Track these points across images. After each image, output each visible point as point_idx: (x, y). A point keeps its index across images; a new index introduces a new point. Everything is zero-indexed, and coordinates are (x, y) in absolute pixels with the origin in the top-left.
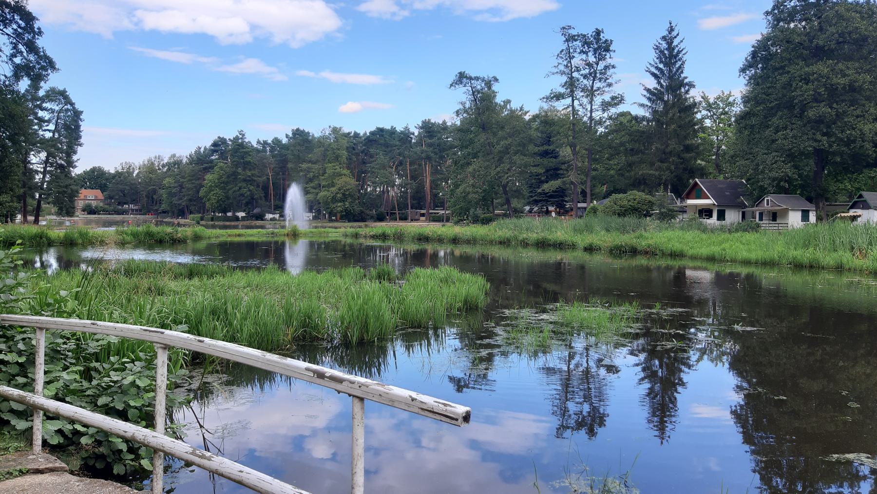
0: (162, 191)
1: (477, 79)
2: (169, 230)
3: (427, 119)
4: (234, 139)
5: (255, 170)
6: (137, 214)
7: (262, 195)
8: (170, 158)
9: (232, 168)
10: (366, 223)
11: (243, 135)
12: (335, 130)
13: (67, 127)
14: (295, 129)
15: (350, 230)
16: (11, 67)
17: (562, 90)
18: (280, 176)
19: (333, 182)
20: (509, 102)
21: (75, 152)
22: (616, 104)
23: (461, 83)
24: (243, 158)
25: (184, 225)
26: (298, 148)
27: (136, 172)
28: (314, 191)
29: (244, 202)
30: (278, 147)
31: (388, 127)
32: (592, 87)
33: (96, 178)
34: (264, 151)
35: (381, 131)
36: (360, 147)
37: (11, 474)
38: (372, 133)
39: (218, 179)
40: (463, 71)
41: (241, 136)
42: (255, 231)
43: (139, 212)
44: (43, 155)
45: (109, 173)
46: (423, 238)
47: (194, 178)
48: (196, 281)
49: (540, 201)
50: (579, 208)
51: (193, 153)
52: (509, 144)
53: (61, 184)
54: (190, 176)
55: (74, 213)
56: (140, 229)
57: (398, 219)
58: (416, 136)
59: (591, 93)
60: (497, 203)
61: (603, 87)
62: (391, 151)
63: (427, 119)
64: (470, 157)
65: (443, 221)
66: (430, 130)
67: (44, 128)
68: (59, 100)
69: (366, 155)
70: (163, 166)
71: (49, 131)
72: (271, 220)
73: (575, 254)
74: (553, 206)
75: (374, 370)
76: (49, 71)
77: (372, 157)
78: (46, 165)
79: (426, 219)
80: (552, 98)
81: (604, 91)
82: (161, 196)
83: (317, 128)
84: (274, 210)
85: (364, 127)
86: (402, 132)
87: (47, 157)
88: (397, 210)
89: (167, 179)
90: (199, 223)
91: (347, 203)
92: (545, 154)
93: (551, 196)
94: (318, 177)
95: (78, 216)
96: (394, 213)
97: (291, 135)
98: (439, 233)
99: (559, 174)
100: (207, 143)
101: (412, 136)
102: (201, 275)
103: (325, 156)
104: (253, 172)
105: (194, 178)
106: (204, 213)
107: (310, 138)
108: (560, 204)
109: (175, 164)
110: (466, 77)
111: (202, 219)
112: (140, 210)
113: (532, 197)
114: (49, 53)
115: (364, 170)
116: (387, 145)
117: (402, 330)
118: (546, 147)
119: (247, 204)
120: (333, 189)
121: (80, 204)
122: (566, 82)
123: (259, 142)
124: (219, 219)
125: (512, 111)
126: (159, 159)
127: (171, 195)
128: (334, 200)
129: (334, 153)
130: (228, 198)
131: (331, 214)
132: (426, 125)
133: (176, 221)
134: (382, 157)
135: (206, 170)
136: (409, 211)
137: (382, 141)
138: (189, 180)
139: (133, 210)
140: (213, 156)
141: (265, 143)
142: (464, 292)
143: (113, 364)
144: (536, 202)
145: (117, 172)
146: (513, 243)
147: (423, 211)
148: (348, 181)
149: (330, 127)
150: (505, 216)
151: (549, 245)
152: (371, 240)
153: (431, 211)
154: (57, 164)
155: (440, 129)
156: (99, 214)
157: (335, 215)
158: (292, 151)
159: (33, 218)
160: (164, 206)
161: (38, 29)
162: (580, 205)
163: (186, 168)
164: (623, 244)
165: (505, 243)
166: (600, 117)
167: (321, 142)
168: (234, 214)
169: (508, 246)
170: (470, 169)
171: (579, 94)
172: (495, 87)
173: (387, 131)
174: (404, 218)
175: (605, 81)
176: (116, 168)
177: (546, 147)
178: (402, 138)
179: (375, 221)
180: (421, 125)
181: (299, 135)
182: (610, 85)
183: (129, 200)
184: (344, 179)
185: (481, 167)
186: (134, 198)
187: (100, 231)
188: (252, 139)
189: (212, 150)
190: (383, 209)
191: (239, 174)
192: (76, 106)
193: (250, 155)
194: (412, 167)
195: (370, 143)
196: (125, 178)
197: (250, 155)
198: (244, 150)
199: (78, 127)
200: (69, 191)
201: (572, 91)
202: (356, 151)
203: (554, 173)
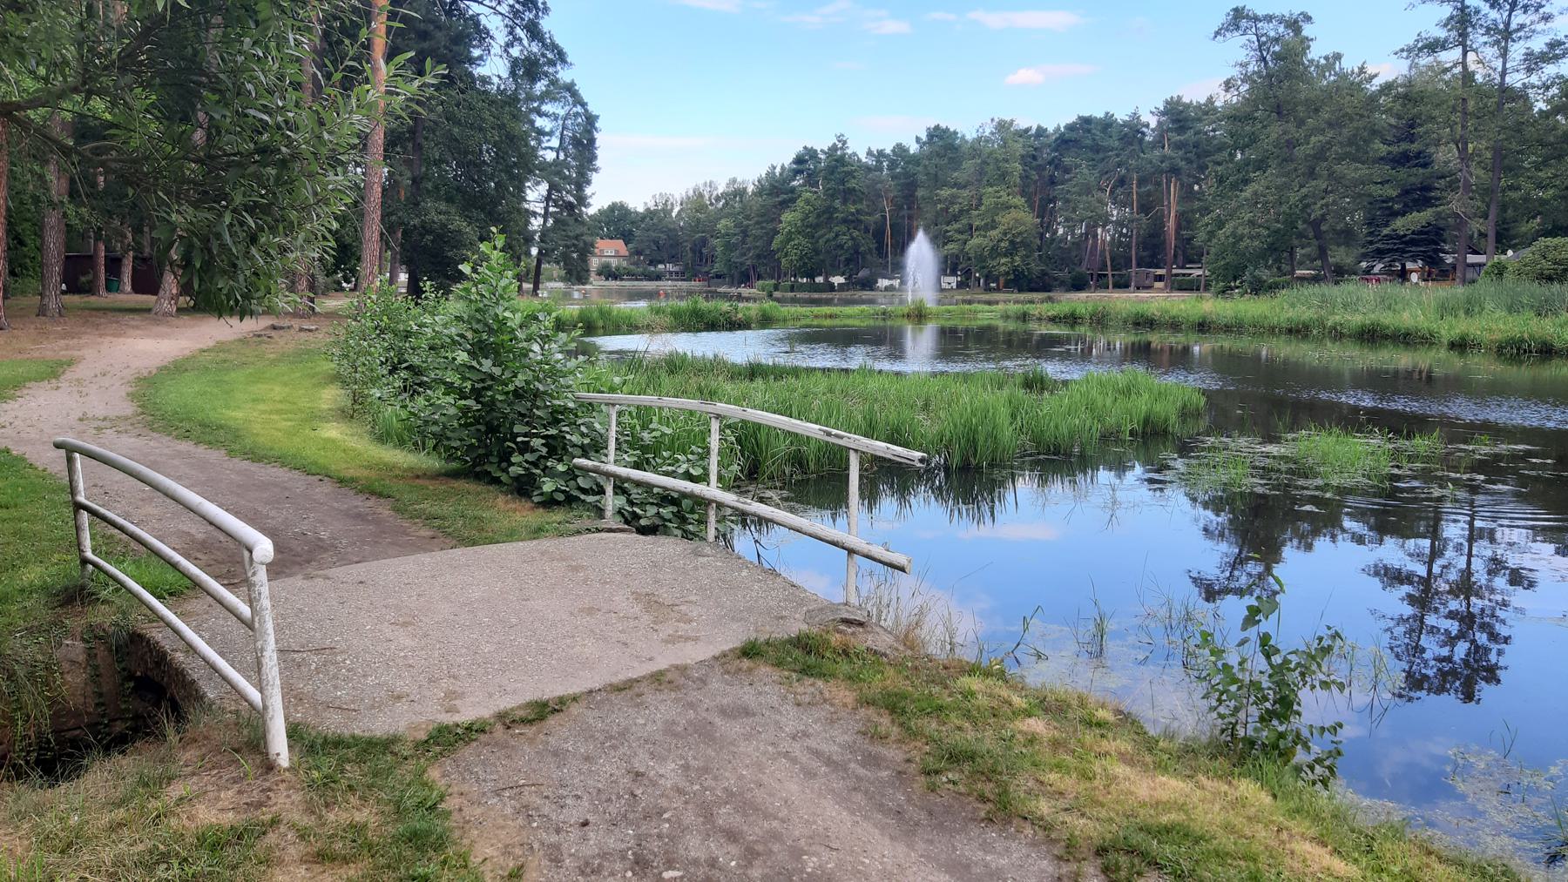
0: (716, 242)
1: (1269, 18)
2: (725, 306)
3: (1175, 96)
4: (829, 149)
5: (861, 203)
6: (677, 280)
7: (873, 246)
8: (728, 185)
9: (825, 200)
10: (1051, 294)
11: (845, 143)
12: (1003, 126)
13: (576, 142)
14: (933, 126)
15: (1013, 308)
16: (506, 62)
17: (1442, 34)
18: (905, 212)
19: (993, 221)
20: (1338, 57)
21: (589, 182)
22: (1557, 58)
23: (1238, 28)
24: (843, 182)
25: (747, 299)
26: (936, 161)
27: (676, 209)
28: (960, 237)
29: (842, 258)
30: (902, 160)
31: (1100, 114)
32: (1507, 24)
33: (618, 221)
34: (879, 168)
35: (1086, 121)
36: (1046, 155)
37: (590, 530)
38: (1070, 128)
39: (802, 220)
40: (1240, 5)
41: (840, 145)
42: (856, 309)
43: (681, 276)
44: (544, 188)
45: (636, 212)
46: (1144, 322)
47: (766, 218)
48: (759, 382)
49: (1389, 251)
50: (1473, 265)
51: (764, 176)
52: (1328, 143)
53: (570, 234)
54: (758, 215)
55: (587, 279)
56: (683, 304)
57: (1111, 286)
58: (1152, 130)
59: (1504, 36)
60: (1304, 255)
61: (1532, 23)
62: (1103, 159)
63: (1175, 96)
64: (1250, 169)
65: (1198, 289)
66: (1180, 118)
67: (543, 145)
68: (565, 97)
69: (1056, 168)
70: (718, 199)
71: (551, 148)
72: (887, 289)
73: (1432, 353)
74: (1415, 261)
75: (985, 508)
76: (559, 67)
77: (1067, 170)
78: (547, 204)
79: (1166, 286)
80: (1420, 50)
81: (1534, 31)
82: (714, 249)
83: (969, 124)
84: (893, 271)
85: (1054, 116)
86: (1125, 124)
87: (549, 191)
88: (1109, 268)
89: (723, 222)
90: (771, 296)
91: (1017, 258)
92: (1402, 160)
93: (1413, 242)
94: (968, 211)
95: (591, 283)
96: (1106, 275)
97: (924, 138)
98: (1174, 312)
99: (1431, 198)
100: (784, 158)
101: (1144, 129)
102: (767, 375)
103: (981, 173)
104: (859, 206)
105: (766, 218)
106: (779, 278)
107: (958, 142)
108: (1430, 257)
109: (737, 193)
110: (1247, 17)
111: (776, 288)
113: (1371, 243)
114: (558, 41)
115: (1051, 197)
116: (1096, 149)
117: (1030, 455)
118: (1404, 146)
119: (848, 261)
120: (993, 233)
121: (595, 263)
122: (1452, 18)
123: (870, 153)
124: (802, 288)
125: (1343, 76)
126: (710, 186)
127: (729, 247)
128: (995, 252)
129: (999, 168)
130: (817, 252)
131: (989, 278)
132: (1173, 109)
133: (733, 291)
134: (1085, 171)
135: (784, 205)
136: (1134, 269)
137: (1088, 142)
138: (757, 223)
139: (671, 273)
140: (794, 180)
141: (881, 153)
143: (665, 459)
144: (1380, 254)
145: (648, 210)
146: (1315, 332)
147: (1160, 272)
148: (1021, 217)
149: (992, 120)
150: (1315, 279)
151: (1386, 337)
152: (1049, 326)
153: (1174, 271)
154: (564, 201)
155: (1200, 113)
156: (622, 280)
157: (996, 280)
158: (925, 166)
159: (531, 286)
160: (718, 267)
161: (543, 3)
162: (1471, 259)
163: (753, 202)
164: (1526, 336)
165: (1298, 331)
166: (1524, 84)
167: (977, 148)
168: (826, 279)
169: (1305, 337)
170: (1248, 192)
171: (1478, 38)
172: (1307, 30)
173: (1099, 122)
174: (1122, 285)
175: (1537, 10)
176: (646, 204)
177: (1404, 146)
178: (1126, 134)
179: (1068, 291)
180: (1162, 108)
181: (941, 141)
182: (1547, 18)
183: (666, 256)
184: (1014, 214)
185: (1268, 188)
186: (674, 252)
187: (624, 307)
188: (859, 148)
189: (794, 170)
190: (1084, 269)
191: (836, 210)
192: (590, 108)
193: (854, 177)
194: (1143, 190)
195: (1064, 147)
196: (661, 220)
197: (854, 177)
198: (846, 169)
199: (592, 141)
200: (581, 245)
201: (1463, 35)
202: (1040, 161)
203: (1420, 197)
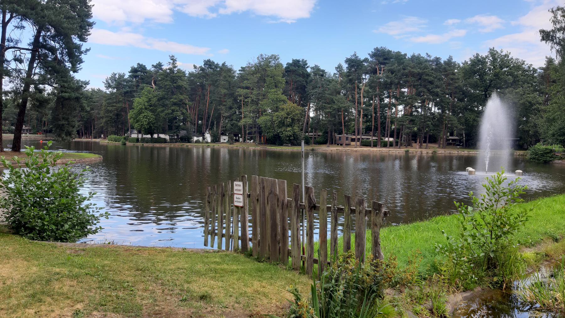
112: (30, 130)
142: (390, 311)
